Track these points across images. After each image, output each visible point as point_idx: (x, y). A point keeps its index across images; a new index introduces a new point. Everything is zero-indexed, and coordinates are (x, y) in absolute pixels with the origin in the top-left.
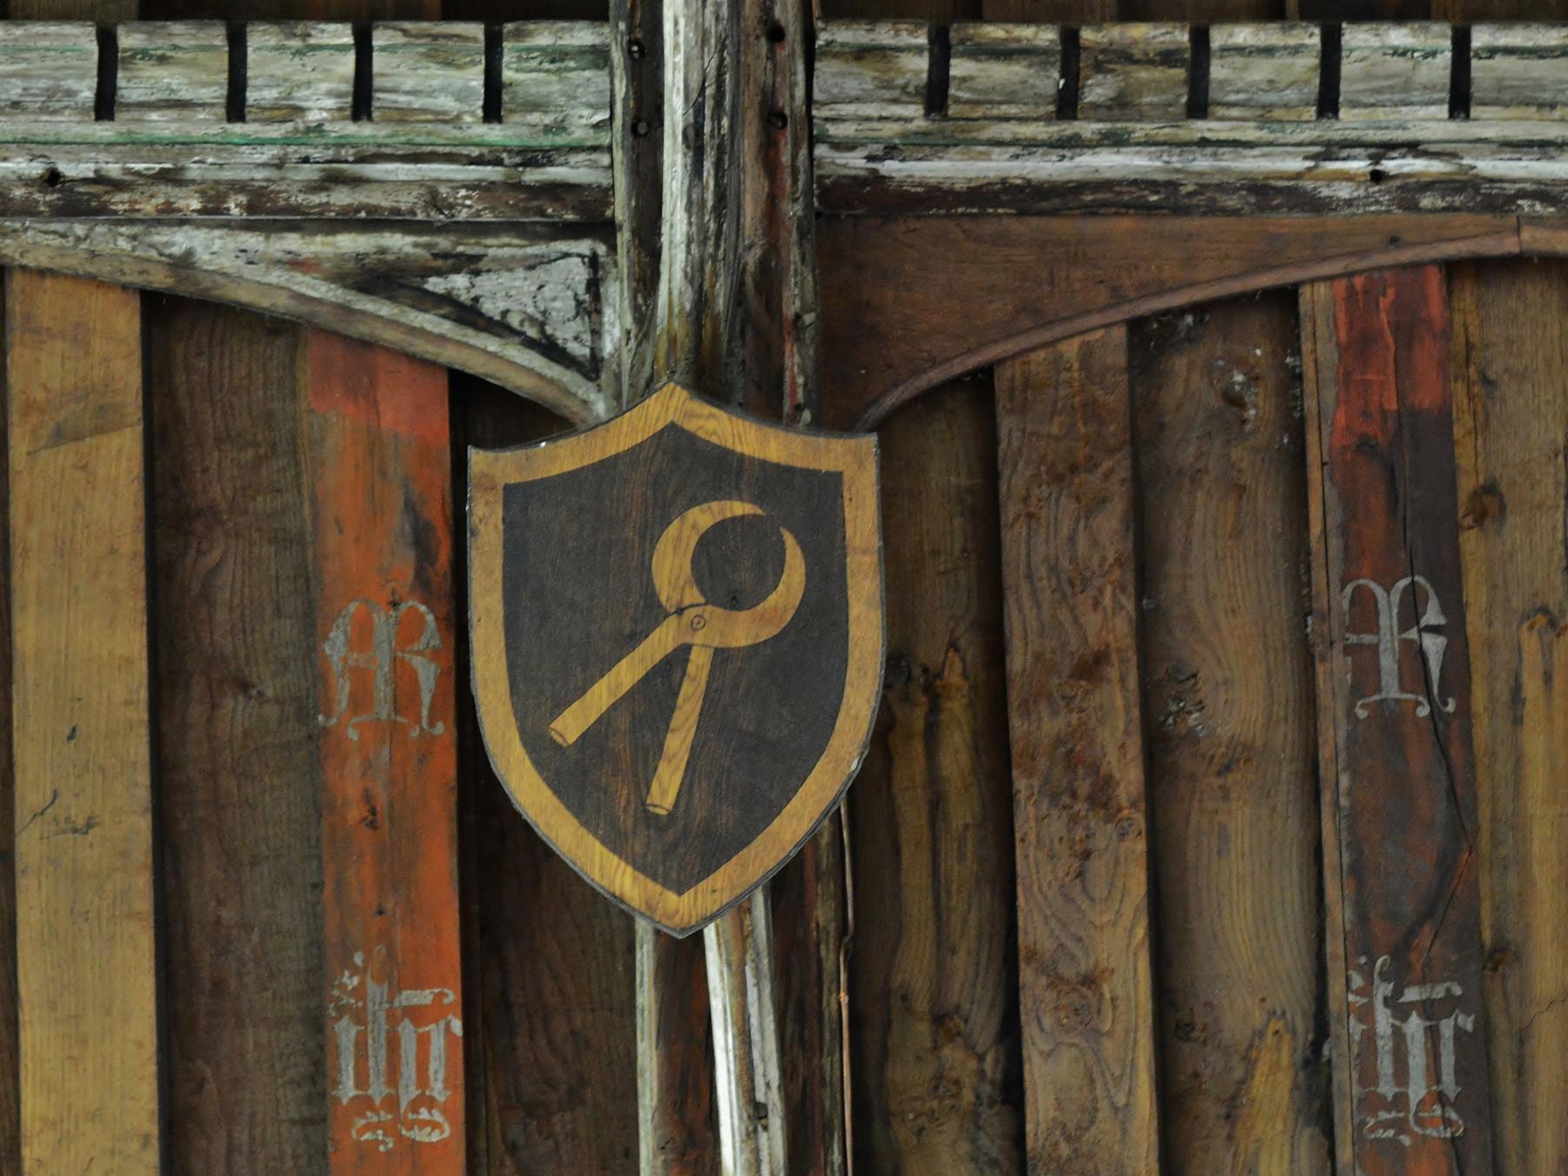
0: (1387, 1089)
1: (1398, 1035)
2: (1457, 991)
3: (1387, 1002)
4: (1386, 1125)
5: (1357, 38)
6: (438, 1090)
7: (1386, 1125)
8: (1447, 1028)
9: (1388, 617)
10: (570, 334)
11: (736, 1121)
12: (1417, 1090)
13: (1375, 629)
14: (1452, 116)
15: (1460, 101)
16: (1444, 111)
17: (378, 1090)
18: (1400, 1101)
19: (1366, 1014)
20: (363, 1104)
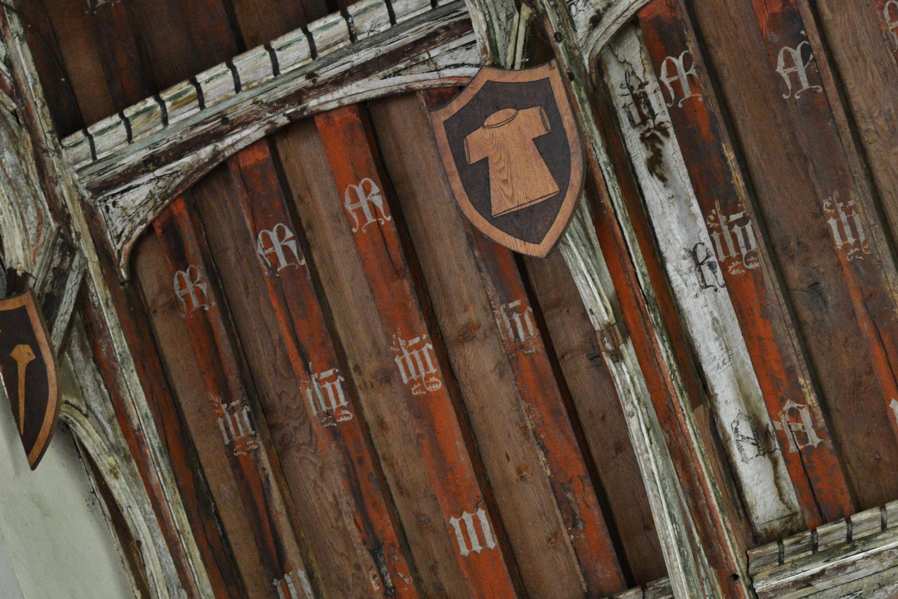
6: (433, 370)
8: (424, 350)
18: (740, 257)
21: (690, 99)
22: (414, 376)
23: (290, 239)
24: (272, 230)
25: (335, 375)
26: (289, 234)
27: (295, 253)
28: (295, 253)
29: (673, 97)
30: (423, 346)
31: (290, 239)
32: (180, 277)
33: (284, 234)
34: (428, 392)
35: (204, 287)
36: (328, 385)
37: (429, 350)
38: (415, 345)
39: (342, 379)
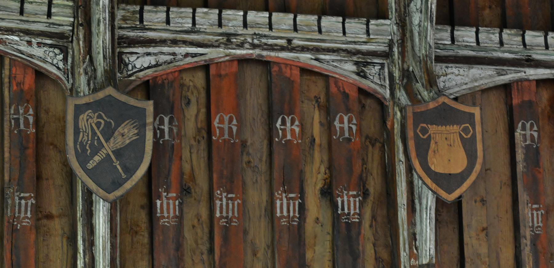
0: (17, 215)
1: (20, 204)
2: (32, 195)
3: (225, 197)
4: (346, 219)
5: (300, 18)
6: (29, 215)
7: (346, 219)
8: (236, 203)
9: (288, 124)
10: (61, 65)
11: (97, 221)
12: (172, 215)
13: (164, 125)
14: (47, 18)
15: (271, 28)
16: (46, 17)
17: (224, 214)
18: (349, 214)
19: (221, 200)
20: (222, 217)
21: (289, 140)
22: (346, 211)
23: (535, 131)
24: (527, 122)
25: (30, 197)
26: (31, 111)
27: (354, 132)
28: (354, 132)
29: (218, 135)
30: (236, 200)
31: (535, 131)
32: (341, 117)
33: (352, 120)
34: (351, 221)
35: (354, 128)
36: (23, 202)
37: (32, 203)
38: (292, 197)
39: (34, 202)
